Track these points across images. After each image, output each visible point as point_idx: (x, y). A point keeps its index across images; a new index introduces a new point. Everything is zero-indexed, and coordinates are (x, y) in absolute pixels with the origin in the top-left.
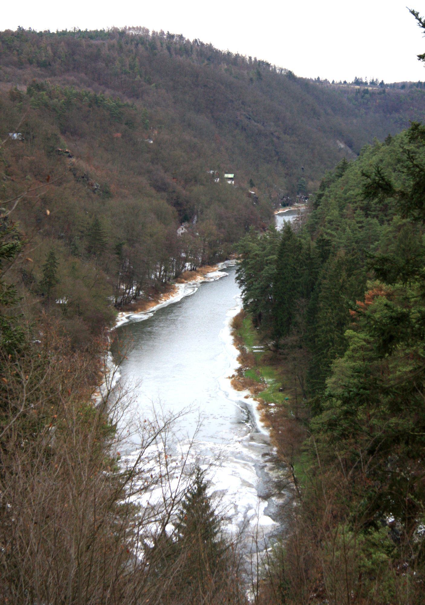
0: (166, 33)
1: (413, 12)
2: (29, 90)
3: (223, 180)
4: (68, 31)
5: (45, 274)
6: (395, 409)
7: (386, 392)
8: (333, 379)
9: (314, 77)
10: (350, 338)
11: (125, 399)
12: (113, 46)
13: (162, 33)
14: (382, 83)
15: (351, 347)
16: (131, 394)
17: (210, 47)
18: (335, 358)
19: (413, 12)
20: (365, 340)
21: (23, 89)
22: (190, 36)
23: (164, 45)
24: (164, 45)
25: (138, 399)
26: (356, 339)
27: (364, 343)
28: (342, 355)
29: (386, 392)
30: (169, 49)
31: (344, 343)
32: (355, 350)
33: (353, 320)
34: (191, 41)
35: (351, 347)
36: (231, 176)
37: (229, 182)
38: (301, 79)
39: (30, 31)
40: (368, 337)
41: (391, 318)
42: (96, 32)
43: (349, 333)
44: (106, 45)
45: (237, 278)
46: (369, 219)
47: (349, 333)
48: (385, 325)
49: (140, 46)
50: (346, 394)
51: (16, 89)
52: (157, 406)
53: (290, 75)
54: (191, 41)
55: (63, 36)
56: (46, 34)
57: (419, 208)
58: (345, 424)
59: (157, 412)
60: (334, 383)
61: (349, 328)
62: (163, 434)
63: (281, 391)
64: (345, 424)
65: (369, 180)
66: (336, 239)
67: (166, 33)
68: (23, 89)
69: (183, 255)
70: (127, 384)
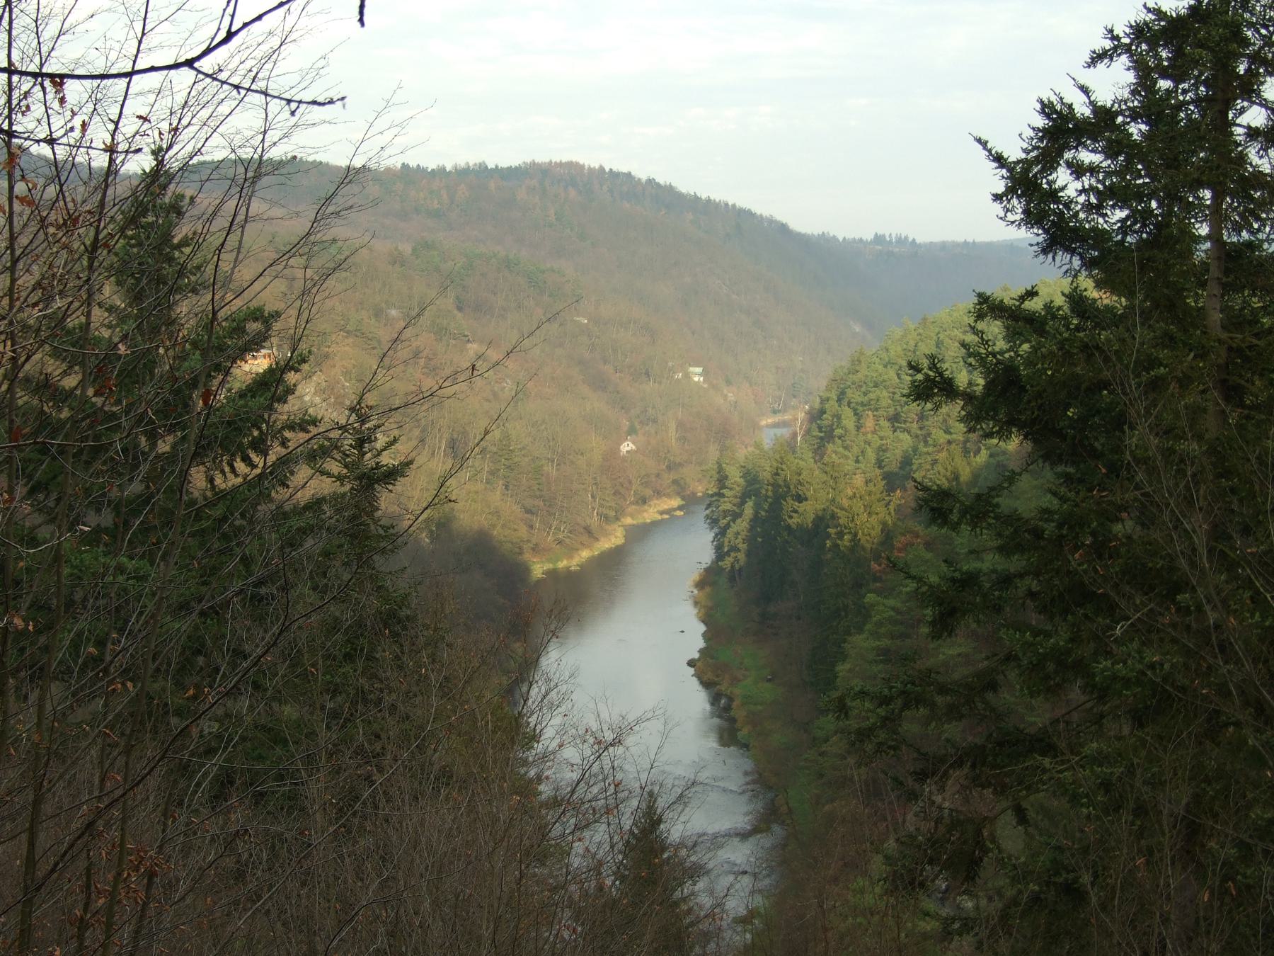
1: (979, 141)
2: (414, 250)
3: (687, 376)
6: (953, 713)
7: (943, 690)
8: (847, 666)
10: (872, 605)
11: (553, 694)
13: (602, 169)
15: (875, 619)
16: (563, 688)
18: (850, 634)
19: (979, 141)
20: (893, 609)
22: (642, 174)
25: (574, 697)
26: (881, 608)
27: (892, 613)
28: (860, 630)
29: (943, 690)
31: (864, 613)
32: (880, 624)
33: (876, 579)
35: (875, 619)
36: (699, 370)
38: (799, 234)
39: (1134, 68)
40: (899, 605)
41: (953, 580)
42: (510, 168)
43: (870, 598)
45: (707, 517)
46: (898, 433)
47: (870, 598)
48: (943, 592)
49: (570, 188)
50: (886, 691)
51: (396, 249)
52: (602, 707)
55: (463, 173)
56: (440, 172)
57: (993, 418)
58: (882, 736)
59: (602, 716)
60: (850, 671)
61: (870, 592)
62: (611, 749)
63: (769, 680)
64: (882, 736)
65: (920, 377)
68: (406, 248)
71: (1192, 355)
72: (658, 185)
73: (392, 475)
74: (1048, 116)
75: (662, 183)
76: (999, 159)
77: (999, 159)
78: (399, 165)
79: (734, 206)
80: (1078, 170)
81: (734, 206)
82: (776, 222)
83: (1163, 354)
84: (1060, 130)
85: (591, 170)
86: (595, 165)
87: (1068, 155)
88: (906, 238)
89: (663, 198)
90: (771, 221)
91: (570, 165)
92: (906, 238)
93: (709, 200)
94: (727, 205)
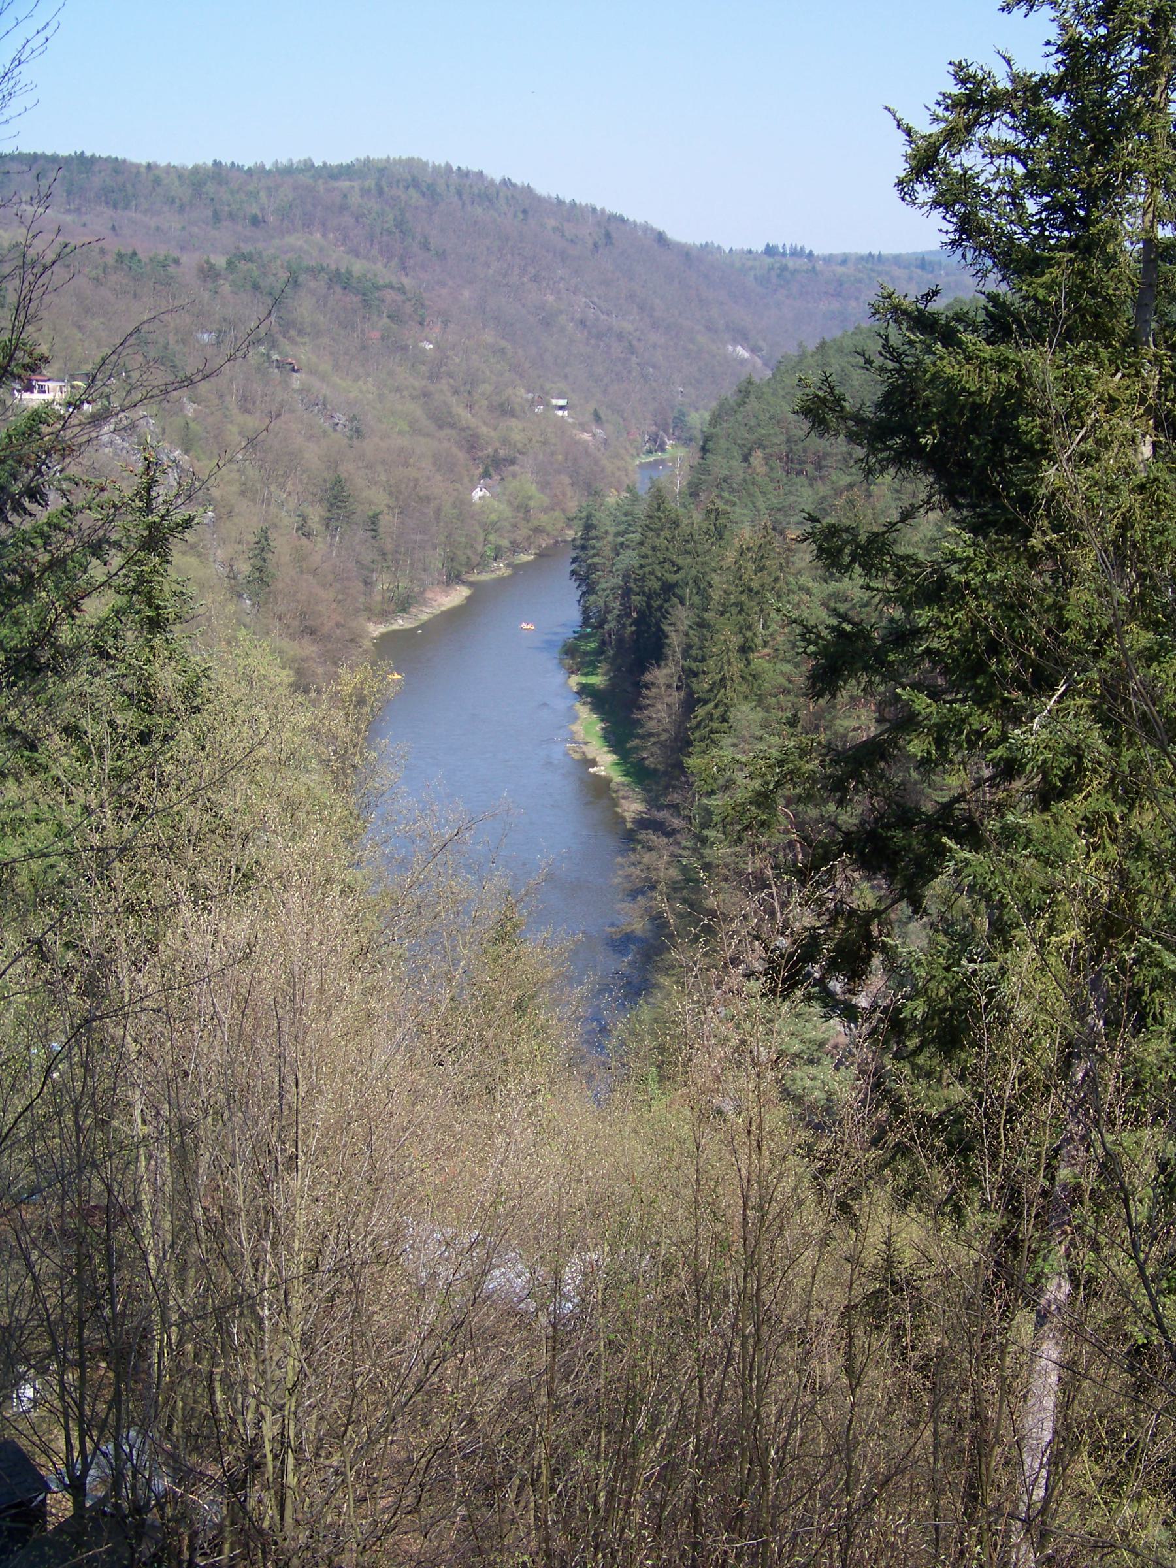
0: (455, 168)
2: (229, 263)
4: (295, 161)
5: (253, 566)
9: (699, 241)
12: (369, 190)
13: (448, 167)
14: (811, 254)
17: (528, 190)
21: (220, 261)
22: (495, 174)
23: (452, 189)
24: (452, 189)
30: (459, 194)
34: (498, 180)
37: (560, 413)
42: (341, 166)
44: (357, 189)
51: (208, 262)
53: (661, 238)
54: (498, 180)
66: (737, 509)
67: (455, 168)
68: (220, 261)
69: (1059, 106)
70: (301, 1200)
71: (1119, 375)
72: (515, 185)
73: (830, 1096)
74: (963, 82)
75: (519, 183)
76: (908, 132)
77: (908, 132)
78: (210, 163)
79: (603, 211)
80: (995, 150)
81: (603, 211)
82: (652, 229)
83: (923, 616)
84: (974, 101)
85: (436, 169)
86: (440, 161)
87: (979, 133)
88: (802, 249)
89: (523, 202)
90: (647, 229)
91: (410, 161)
92: (802, 249)
93: (573, 204)
94: (594, 210)
